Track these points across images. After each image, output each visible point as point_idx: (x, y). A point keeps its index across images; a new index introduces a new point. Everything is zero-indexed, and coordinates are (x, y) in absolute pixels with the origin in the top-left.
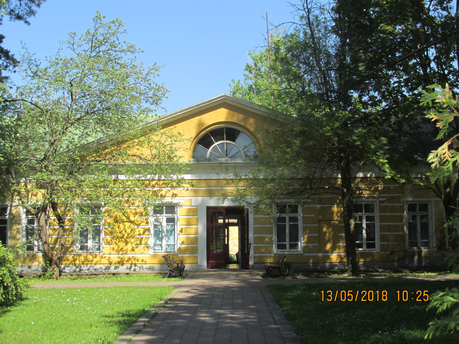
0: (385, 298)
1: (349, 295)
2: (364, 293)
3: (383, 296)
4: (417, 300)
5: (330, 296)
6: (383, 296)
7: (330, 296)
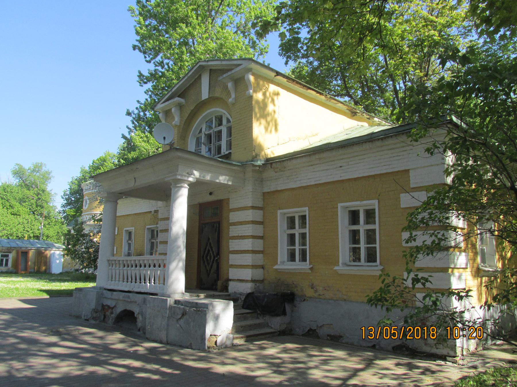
0: (433, 335)
1: (393, 331)
2: (410, 330)
3: (432, 333)
4: (408, 338)
5: (372, 333)
6: (432, 333)
7: (372, 333)
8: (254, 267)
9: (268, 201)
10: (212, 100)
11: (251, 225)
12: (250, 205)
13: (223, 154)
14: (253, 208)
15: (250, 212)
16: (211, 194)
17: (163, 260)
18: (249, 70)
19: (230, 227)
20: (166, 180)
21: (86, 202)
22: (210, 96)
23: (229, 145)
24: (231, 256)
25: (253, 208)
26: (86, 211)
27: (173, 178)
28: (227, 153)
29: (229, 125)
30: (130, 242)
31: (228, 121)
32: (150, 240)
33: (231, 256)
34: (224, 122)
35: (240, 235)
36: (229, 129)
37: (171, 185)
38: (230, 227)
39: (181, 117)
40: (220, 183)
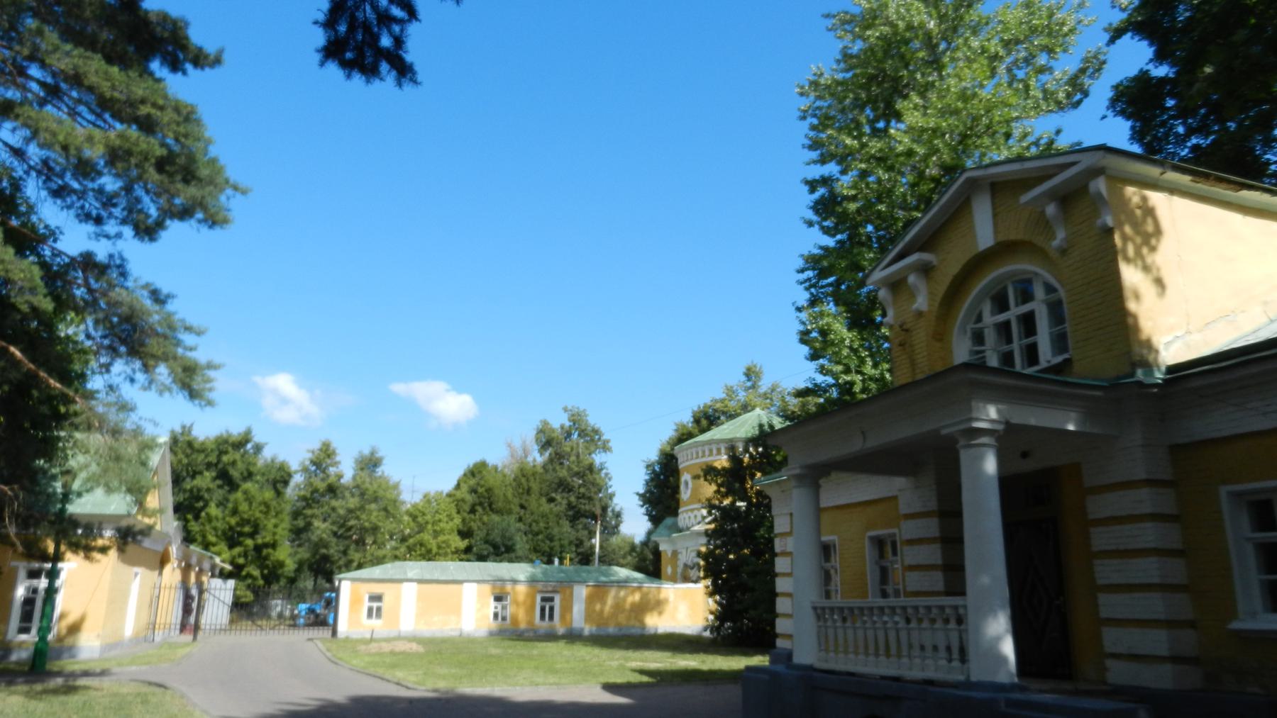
8: (1170, 624)
9: (1188, 468)
10: (1003, 250)
11: (1149, 525)
12: (1143, 476)
13: (1043, 364)
14: (1149, 482)
15: (1144, 493)
16: (1025, 455)
17: (956, 608)
18: (1098, 172)
19: (1092, 530)
20: (944, 432)
21: (686, 483)
22: (1001, 238)
23: (1060, 342)
24: (1103, 599)
25: (1149, 482)
26: (686, 504)
27: (962, 427)
28: (1059, 359)
29: (1053, 296)
30: (828, 565)
31: (1050, 289)
32: (877, 563)
33: (1103, 599)
34: (1039, 292)
35: (1122, 547)
36: (1056, 310)
37: (957, 442)
38: (1092, 530)
39: (931, 294)
40: (459, 388)
